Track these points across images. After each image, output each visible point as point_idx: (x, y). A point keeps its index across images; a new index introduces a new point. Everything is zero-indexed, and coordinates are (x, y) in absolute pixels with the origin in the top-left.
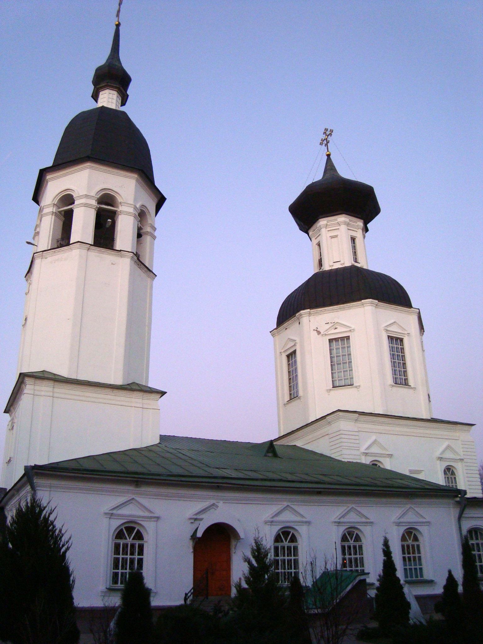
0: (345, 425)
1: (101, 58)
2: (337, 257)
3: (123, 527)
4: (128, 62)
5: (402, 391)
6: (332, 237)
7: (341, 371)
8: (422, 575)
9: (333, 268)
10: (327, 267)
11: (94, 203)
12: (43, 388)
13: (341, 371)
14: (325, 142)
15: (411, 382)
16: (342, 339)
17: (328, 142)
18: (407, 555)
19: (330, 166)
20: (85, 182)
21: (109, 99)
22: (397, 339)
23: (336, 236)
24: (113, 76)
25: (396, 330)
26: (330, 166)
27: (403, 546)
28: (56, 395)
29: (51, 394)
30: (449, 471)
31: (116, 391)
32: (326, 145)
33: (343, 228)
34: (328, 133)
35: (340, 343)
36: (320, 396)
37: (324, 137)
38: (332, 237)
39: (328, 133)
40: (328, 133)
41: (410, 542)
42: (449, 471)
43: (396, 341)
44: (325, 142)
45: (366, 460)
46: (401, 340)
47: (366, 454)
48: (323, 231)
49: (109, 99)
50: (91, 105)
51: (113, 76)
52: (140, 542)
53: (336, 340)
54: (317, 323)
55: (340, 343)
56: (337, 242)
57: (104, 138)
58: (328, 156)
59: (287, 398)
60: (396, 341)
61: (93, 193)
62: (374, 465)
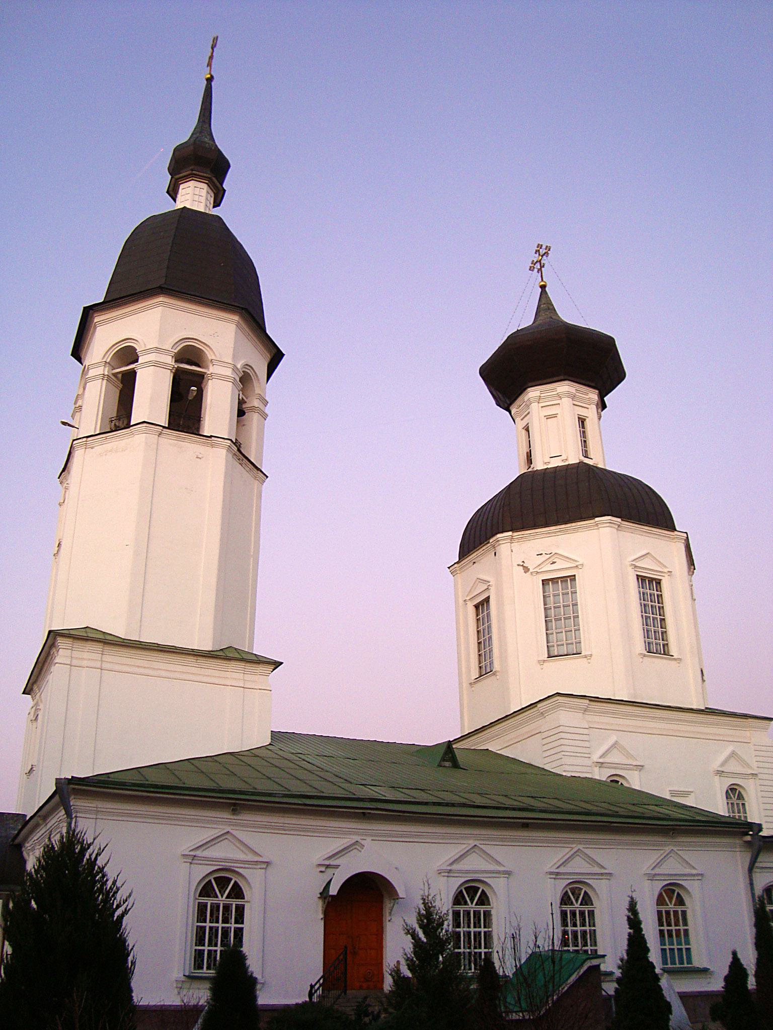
0: (567, 718)
1: (183, 132)
2: (556, 449)
3: (211, 878)
4: (224, 138)
5: (659, 663)
6: (548, 417)
7: (562, 633)
8: (689, 961)
9: (549, 467)
10: (539, 465)
11: (169, 360)
12: (86, 655)
13: (562, 633)
14: (538, 266)
15: (673, 650)
16: (564, 579)
17: (542, 266)
18: (665, 928)
19: (545, 305)
20: (156, 327)
21: (194, 196)
22: (651, 580)
23: (554, 416)
24: (201, 160)
25: (650, 567)
26: (545, 305)
27: (659, 913)
28: (105, 666)
29: (98, 664)
30: (734, 793)
31: (202, 660)
32: (540, 270)
33: (566, 402)
34: (543, 252)
35: (559, 586)
36: (527, 671)
37: (536, 257)
38: (548, 417)
39: (542, 251)
40: (543, 252)
41: (671, 907)
42: (734, 793)
43: (650, 584)
44: (538, 266)
45: (601, 775)
46: (659, 582)
47: (601, 765)
48: (534, 406)
49: (194, 196)
50: (166, 206)
51: (201, 160)
52: (240, 902)
53: (554, 580)
54: (522, 555)
55: (559, 586)
56: (556, 425)
57: (191, 260)
58: (543, 287)
59: (475, 674)
60: (650, 584)
61: (168, 346)
62: (614, 781)
